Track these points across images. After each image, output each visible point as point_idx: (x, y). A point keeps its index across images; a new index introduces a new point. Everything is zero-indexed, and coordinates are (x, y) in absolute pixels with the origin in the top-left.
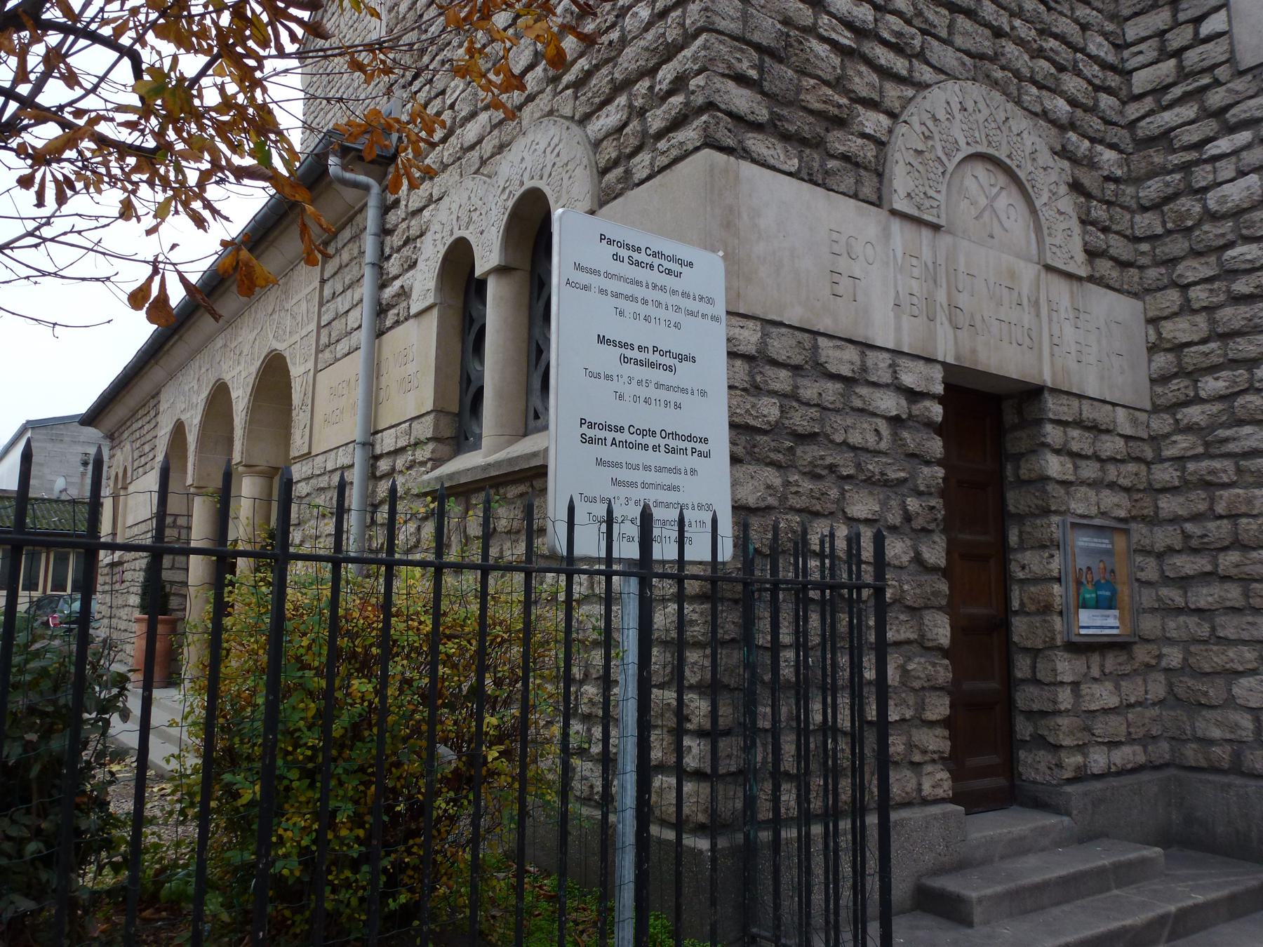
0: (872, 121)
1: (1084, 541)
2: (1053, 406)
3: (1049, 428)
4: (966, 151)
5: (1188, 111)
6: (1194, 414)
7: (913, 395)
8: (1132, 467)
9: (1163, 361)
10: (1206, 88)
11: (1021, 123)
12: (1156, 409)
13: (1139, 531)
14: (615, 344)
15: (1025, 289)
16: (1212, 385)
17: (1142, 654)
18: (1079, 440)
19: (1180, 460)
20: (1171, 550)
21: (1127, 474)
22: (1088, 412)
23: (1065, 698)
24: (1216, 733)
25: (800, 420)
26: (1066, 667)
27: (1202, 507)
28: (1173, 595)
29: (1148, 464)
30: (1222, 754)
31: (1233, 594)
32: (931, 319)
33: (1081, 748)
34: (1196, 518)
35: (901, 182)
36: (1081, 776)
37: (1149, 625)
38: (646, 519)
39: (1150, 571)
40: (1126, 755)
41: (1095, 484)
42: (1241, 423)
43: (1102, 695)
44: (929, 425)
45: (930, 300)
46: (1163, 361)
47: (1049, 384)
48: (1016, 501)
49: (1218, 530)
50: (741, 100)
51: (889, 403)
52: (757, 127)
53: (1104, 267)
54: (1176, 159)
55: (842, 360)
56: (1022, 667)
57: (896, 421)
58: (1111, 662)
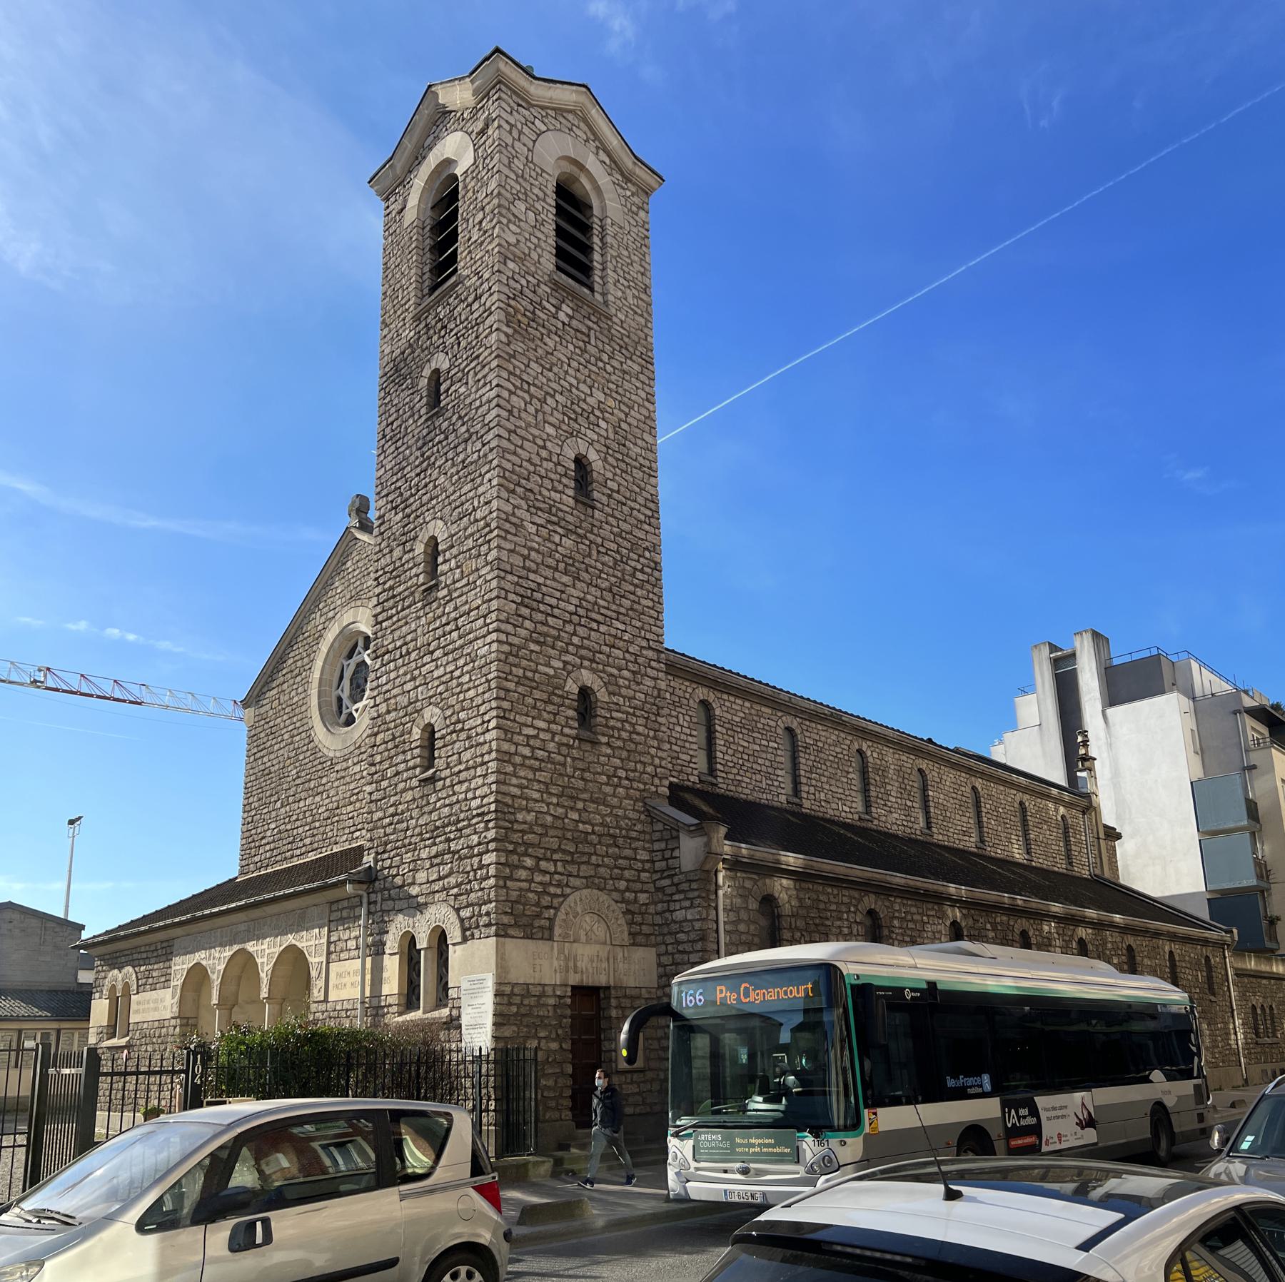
11: (603, 897)
25: (523, 1010)
32: (567, 971)
38: (480, 1049)
45: (567, 967)
46: (661, 970)
48: (604, 1024)
51: (552, 1001)
55: (535, 991)
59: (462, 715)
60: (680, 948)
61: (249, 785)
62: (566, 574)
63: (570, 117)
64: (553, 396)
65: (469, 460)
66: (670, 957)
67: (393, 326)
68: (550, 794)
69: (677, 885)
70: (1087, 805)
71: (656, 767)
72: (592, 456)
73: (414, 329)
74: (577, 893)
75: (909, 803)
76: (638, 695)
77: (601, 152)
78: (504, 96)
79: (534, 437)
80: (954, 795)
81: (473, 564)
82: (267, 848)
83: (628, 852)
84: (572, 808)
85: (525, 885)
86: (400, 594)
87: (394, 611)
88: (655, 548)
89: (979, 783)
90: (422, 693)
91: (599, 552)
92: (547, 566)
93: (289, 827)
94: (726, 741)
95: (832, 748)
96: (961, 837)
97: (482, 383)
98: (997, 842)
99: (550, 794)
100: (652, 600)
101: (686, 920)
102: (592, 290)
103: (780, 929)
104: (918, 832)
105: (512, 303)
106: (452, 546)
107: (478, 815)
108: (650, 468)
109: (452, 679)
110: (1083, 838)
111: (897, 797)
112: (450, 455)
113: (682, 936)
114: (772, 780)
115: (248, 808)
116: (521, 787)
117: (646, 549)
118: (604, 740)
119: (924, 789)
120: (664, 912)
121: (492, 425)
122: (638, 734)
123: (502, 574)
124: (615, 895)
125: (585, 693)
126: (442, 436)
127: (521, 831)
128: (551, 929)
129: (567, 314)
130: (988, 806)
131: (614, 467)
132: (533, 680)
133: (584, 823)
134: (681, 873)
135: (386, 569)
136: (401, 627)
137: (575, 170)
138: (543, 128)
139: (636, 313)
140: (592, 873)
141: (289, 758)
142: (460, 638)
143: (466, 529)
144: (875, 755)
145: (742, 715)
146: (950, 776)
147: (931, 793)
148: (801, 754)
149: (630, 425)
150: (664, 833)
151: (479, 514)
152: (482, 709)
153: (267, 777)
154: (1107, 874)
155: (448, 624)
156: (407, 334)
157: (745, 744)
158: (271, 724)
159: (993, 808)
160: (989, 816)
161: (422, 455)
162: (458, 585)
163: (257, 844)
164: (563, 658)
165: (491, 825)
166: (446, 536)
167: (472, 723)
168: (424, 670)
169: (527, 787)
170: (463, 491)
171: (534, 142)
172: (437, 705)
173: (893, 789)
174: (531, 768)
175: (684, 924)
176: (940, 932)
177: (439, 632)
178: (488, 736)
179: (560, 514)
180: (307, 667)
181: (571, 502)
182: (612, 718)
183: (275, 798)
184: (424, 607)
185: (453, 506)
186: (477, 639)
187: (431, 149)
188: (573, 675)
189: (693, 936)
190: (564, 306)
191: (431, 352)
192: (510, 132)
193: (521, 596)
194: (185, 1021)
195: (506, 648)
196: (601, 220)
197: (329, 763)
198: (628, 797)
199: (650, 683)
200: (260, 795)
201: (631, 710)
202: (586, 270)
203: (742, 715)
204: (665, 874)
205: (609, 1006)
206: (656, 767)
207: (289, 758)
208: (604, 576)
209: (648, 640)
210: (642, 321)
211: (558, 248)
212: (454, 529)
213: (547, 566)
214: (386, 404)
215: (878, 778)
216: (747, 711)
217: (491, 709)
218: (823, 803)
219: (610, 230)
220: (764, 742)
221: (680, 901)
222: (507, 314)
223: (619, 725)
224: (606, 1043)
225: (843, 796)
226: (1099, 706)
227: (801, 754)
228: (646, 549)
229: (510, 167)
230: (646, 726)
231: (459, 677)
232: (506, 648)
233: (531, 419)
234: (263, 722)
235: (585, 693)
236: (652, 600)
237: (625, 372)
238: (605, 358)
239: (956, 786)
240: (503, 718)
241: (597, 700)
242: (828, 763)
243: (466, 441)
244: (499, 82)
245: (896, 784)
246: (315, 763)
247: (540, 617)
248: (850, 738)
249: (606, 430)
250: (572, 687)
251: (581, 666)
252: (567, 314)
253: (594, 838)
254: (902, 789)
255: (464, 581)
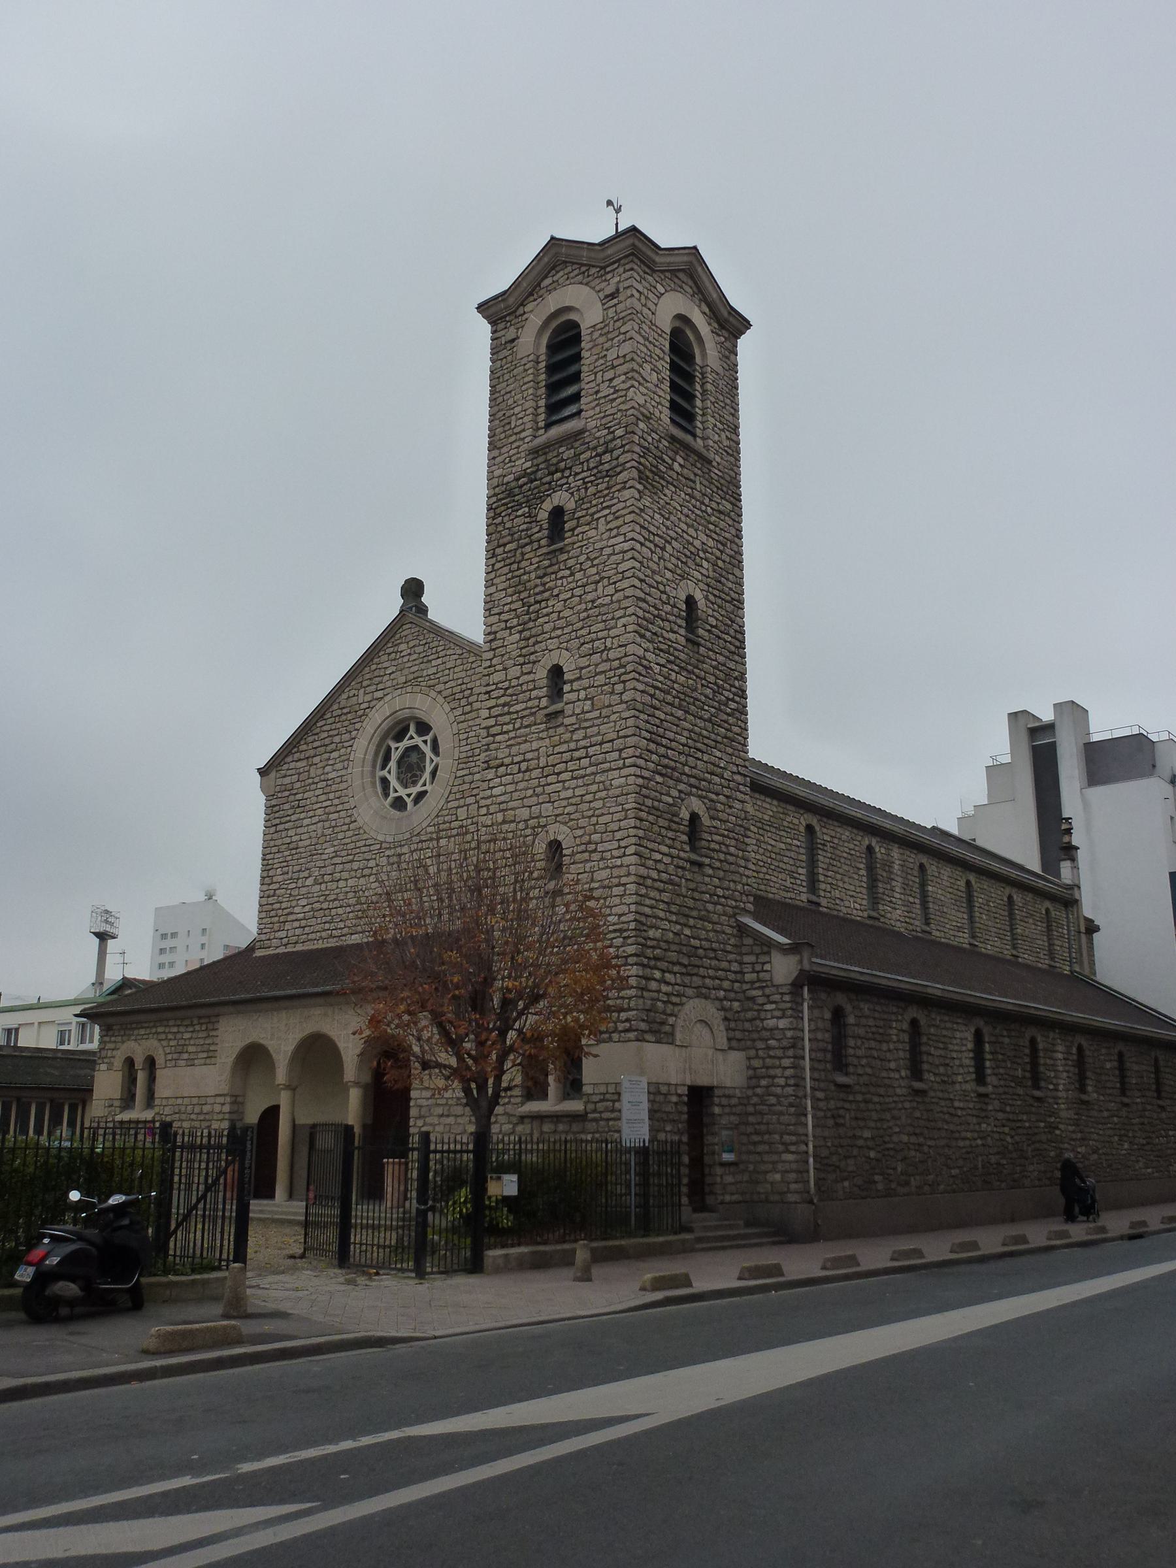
0: (671, 1020)
1: (724, 1133)
2: (717, 1092)
3: (716, 1099)
4: (694, 1020)
5: (760, 993)
6: (759, 1091)
7: (680, 1096)
8: (740, 1107)
9: (751, 1072)
10: (764, 987)
12: (749, 1087)
13: (742, 1128)
14: (1113, 1239)
15: (710, 1057)
16: (764, 1082)
17: (742, 1167)
18: (724, 1101)
19: (755, 1105)
20: (751, 1133)
21: (738, 1110)
22: (727, 1092)
23: (718, 1179)
24: (762, 1191)
26: (719, 1170)
27: (760, 1120)
28: (751, 1148)
29: (745, 1105)
30: (763, 1197)
31: (767, 1148)
33: (723, 1194)
34: (759, 1124)
35: (678, 1036)
36: (722, 1203)
37: (744, 1157)
38: (644, 1141)
39: (745, 1139)
40: (735, 1198)
41: (729, 1114)
42: (769, 1095)
43: (729, 1179)
44: (684, 1103)
46: (751, 1072)
47: (715, 1084)
48: (706, 1120)
49: (763, 1128)
50: (643, 1026)
51: (674, 1099)
52: (646, 1032)
53: (734, 1043)
54: (756, 1007)
56: (707, 1171)
57: (676, 1103)
58: (732, 1169)
59: (596, 837)
60: (772, 1053)
61: (268, 857)
62: (679, 709)
63: (681, 275)
64: (670, 543)
65: (600, 601)
66: (761, 1061)
67: (504, 450)
68: (671, 912)
69: (768, 996)
70: (1068, 900)
71: (744, 885)
72: (698, 595)
73: (532, 459)
74: (691, 1001)
75: (911, 899)
76: (731, 817)
77: (703, 304)
78: (636, 267)
79: (658, 583)
80: (951, 890)
81: (606, 700)
82: (296, 924)
83: (724, 965)
84: (685, 925)
85: (655, 995)
86: (517, 712)
87: (510, 727)
88: (742, 677)
89: (972, 878)
90: (547, 809)
91: (703, 685)
92: (667, 703)
93: (325, 906)
94: (757, 840)
95: (846, 844)
96: (956, 933)
97: (614, 532)
98: (988, 937)
99: (671, 912)
100: (740, 727)
101: (777, 1028)
102: (694, 436)
103: (845, 1036)
104: (918, 929)
105: (642, 460)
106: (580, 678)
107: (615, 931)
108: (739, 601)
109: (582, 802)
110: (1065, 932)
111: (901, 894)
112: (578, 592)
113: (772, 1042)
114: (795, 878)
115: (267, 880)
116: (652, 907)
117: (736, 678)
118: (707, 861)
119: (923, 885)
120: (755, 1019)
121: (627, 574)
122: (732, 855)
123: (637, 713)
124: (717, 1003)
125: (694, 817)
126: (568, 572)
127: (651, 947)
128: (672, 1034)
129: (680, 465)
130: (980, 900)
131: (713, 603)
132: (658, 810)
133: (694, 938)
134: (774, 986)
135: (500, 685)
136: (520, 744)
137: (683, 326)
138: (663, 291)
139: (728, 453)
140: (700, 983)
141: (323, 835)
142: (591, 765)
143: (597, 665)
144: (883, 851)
145: (771, 813)
146: (946, 872)
147: (930, 888)
148: (820, 852)
149: (724, 561)
150: (754, 948)
151: (612, 655)
152: (618, 835)
153: (294, 852)
154: (1087, 972)
155: (577, 750)
156: (523, 464)
157: (773, 843)
158: (299, 797)
159: (985, 902)
160: (981, 911)
161: (544, 585)
162: (588, 716)
163: (282, 919)
164: (679, 788)
165: (630, 941)
166: (574, 667)
167: (607, 846)
168: (549, 789)
169: (655, 908)
170: (593, 629)
171: (656, 305)
172: (565, 823)
173: (898, 885)
174: (657, 889)
175: (776, 1032)
176: (966, 1039)
177: (567, 756)
178: (627, 860)
179: (676, 653)
180: (346, 744)
181: (682, 640)
182: (712, 841)
183: (306, 874)
184: (548, 729)
185: (582, 641)
186: (611, 769)
187: (550, 291)
188: (685, 802)
189: (785, 1043)
190: (678, 457)
191: (552, 488)
192: (639, 300)
193: (650, 732)
194: (234, 1099)
195: (640, 781)
196: (701, 368)
197: (378, 846)
198: (725, 914)
199: (738, 805)
200: (285, 869)
201: (726, 833)
202: (690, 417)
203: (771, 813)
204: (757, 985)
205: (713, 1104)
206: (744, 885)
207: (323, 835)
208: (706, 708)
209: (737, 765)
210: (732, 459)
211: (672, 401)
212: (584, 662)
213: (667, 703)
214: (496, 525)
215: (885, 874)
216: (775, 810)
217: (629, 836)
218: (838, 902)
219: (710, 377)
220: (789, 840)
221: (771, 1010)
222: (639, 471)
223: (717, 847)
224: (709, 1138)
225: (854, 894)
226: (1077, 785)
227: (820, 852)
228: (736, 678)
229: (640, 333)
230: (735, 847)
231: (590, 802)
232: (640, 781)
233: (655, 567)
234: (287, 793)
235: (694, 817)
236: (740, 727)
237: (720, 512)
238: (707, 501)
239: (952, 881)
240: (639, 845)
241: (702, 824)
242: (843, 860)
243: (597, 582)
244: (632, 254)
245: (900, 879)
246: (358, 844)
247: (662, 750)
248: (861, 834)
249: (707, 569)
250: (685, 814)
251: (690, 794)
252: (680, 465)
253: (701, 952)
254: (905, 885)
255: (596, 714)
